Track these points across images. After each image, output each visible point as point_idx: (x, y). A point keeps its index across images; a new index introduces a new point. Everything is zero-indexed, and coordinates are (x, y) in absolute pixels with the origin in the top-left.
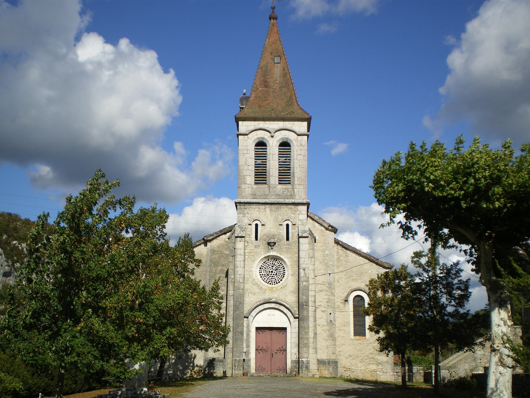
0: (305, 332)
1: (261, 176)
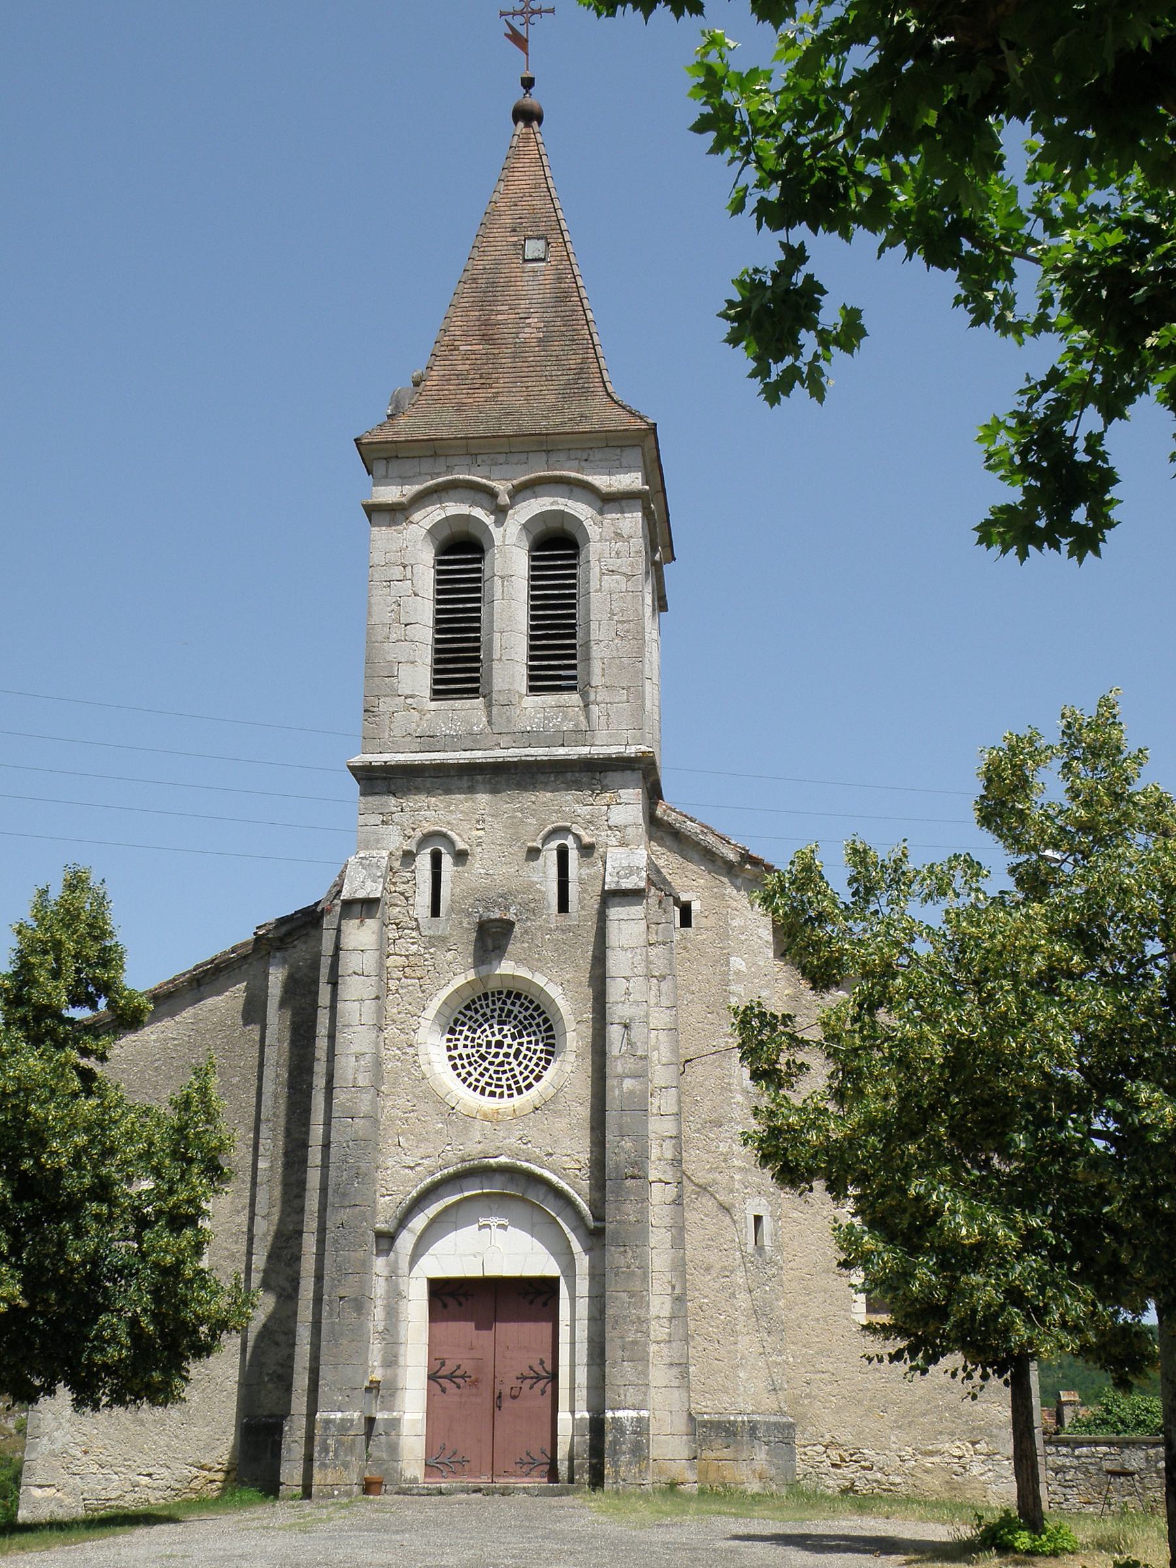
1: (459, 664)
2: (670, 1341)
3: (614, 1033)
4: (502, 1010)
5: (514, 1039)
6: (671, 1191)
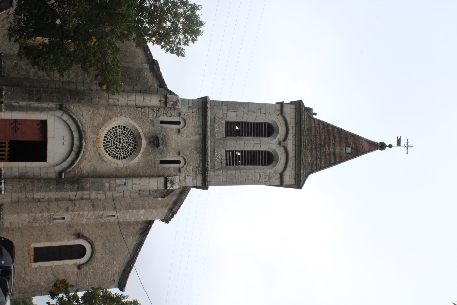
0: (41, 187)
2: (26, 198)
3: (123, 180)
4: (131, 143)
5: (122, 147)
6: (73, 198)
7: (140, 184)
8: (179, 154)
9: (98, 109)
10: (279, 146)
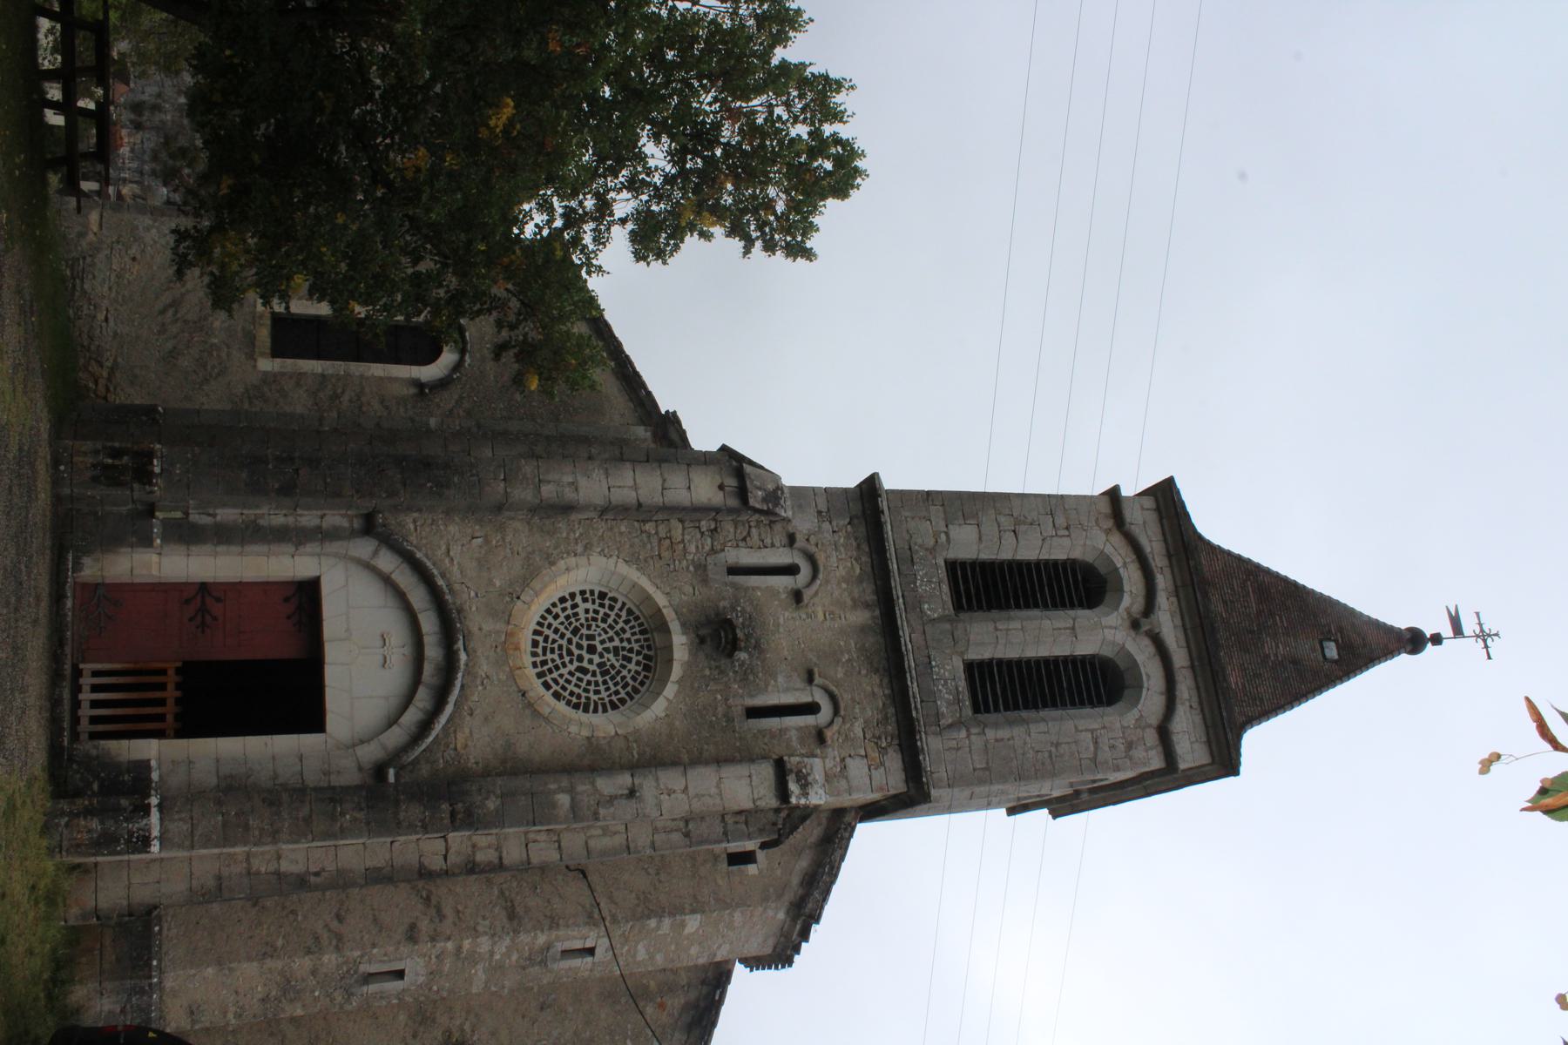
0: (308, 820)
2: (249, 873)
3: (625, 780)
4: (631, 651)
5: (600, 665)
6: (436, 863)
7: (685, 790)
8: (810, 679)
9: (501, 528)
10: (1133, 633)
